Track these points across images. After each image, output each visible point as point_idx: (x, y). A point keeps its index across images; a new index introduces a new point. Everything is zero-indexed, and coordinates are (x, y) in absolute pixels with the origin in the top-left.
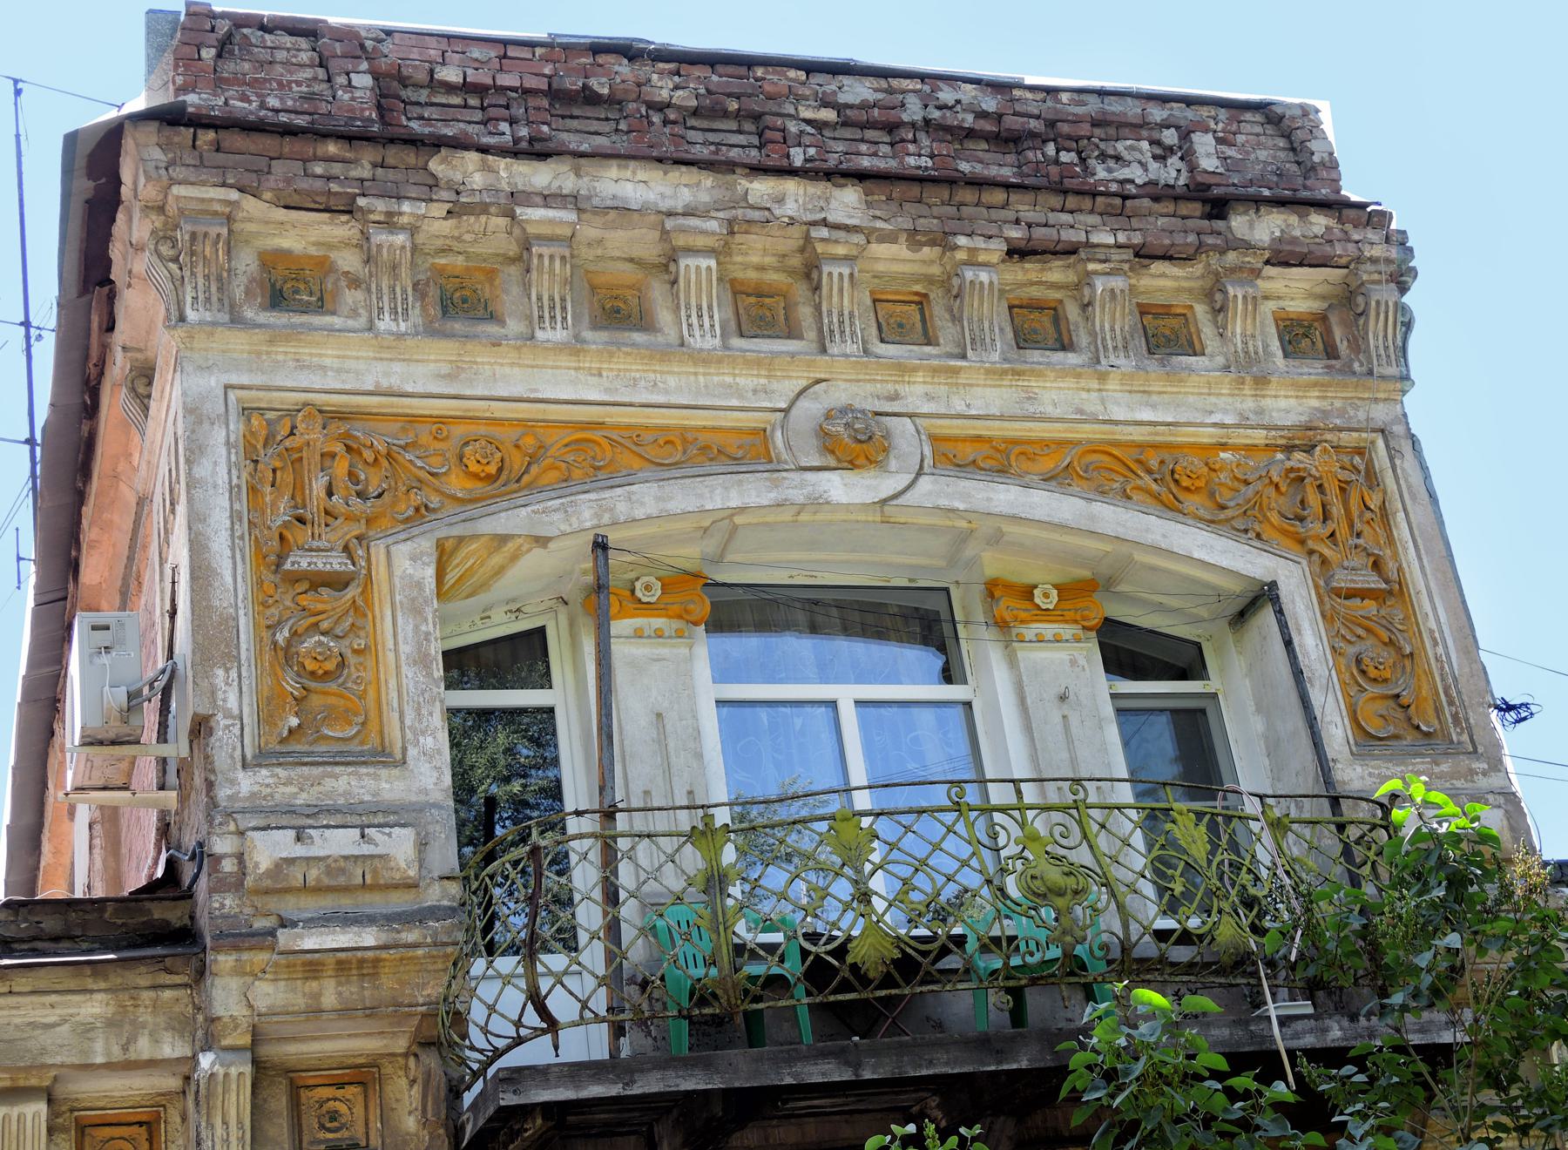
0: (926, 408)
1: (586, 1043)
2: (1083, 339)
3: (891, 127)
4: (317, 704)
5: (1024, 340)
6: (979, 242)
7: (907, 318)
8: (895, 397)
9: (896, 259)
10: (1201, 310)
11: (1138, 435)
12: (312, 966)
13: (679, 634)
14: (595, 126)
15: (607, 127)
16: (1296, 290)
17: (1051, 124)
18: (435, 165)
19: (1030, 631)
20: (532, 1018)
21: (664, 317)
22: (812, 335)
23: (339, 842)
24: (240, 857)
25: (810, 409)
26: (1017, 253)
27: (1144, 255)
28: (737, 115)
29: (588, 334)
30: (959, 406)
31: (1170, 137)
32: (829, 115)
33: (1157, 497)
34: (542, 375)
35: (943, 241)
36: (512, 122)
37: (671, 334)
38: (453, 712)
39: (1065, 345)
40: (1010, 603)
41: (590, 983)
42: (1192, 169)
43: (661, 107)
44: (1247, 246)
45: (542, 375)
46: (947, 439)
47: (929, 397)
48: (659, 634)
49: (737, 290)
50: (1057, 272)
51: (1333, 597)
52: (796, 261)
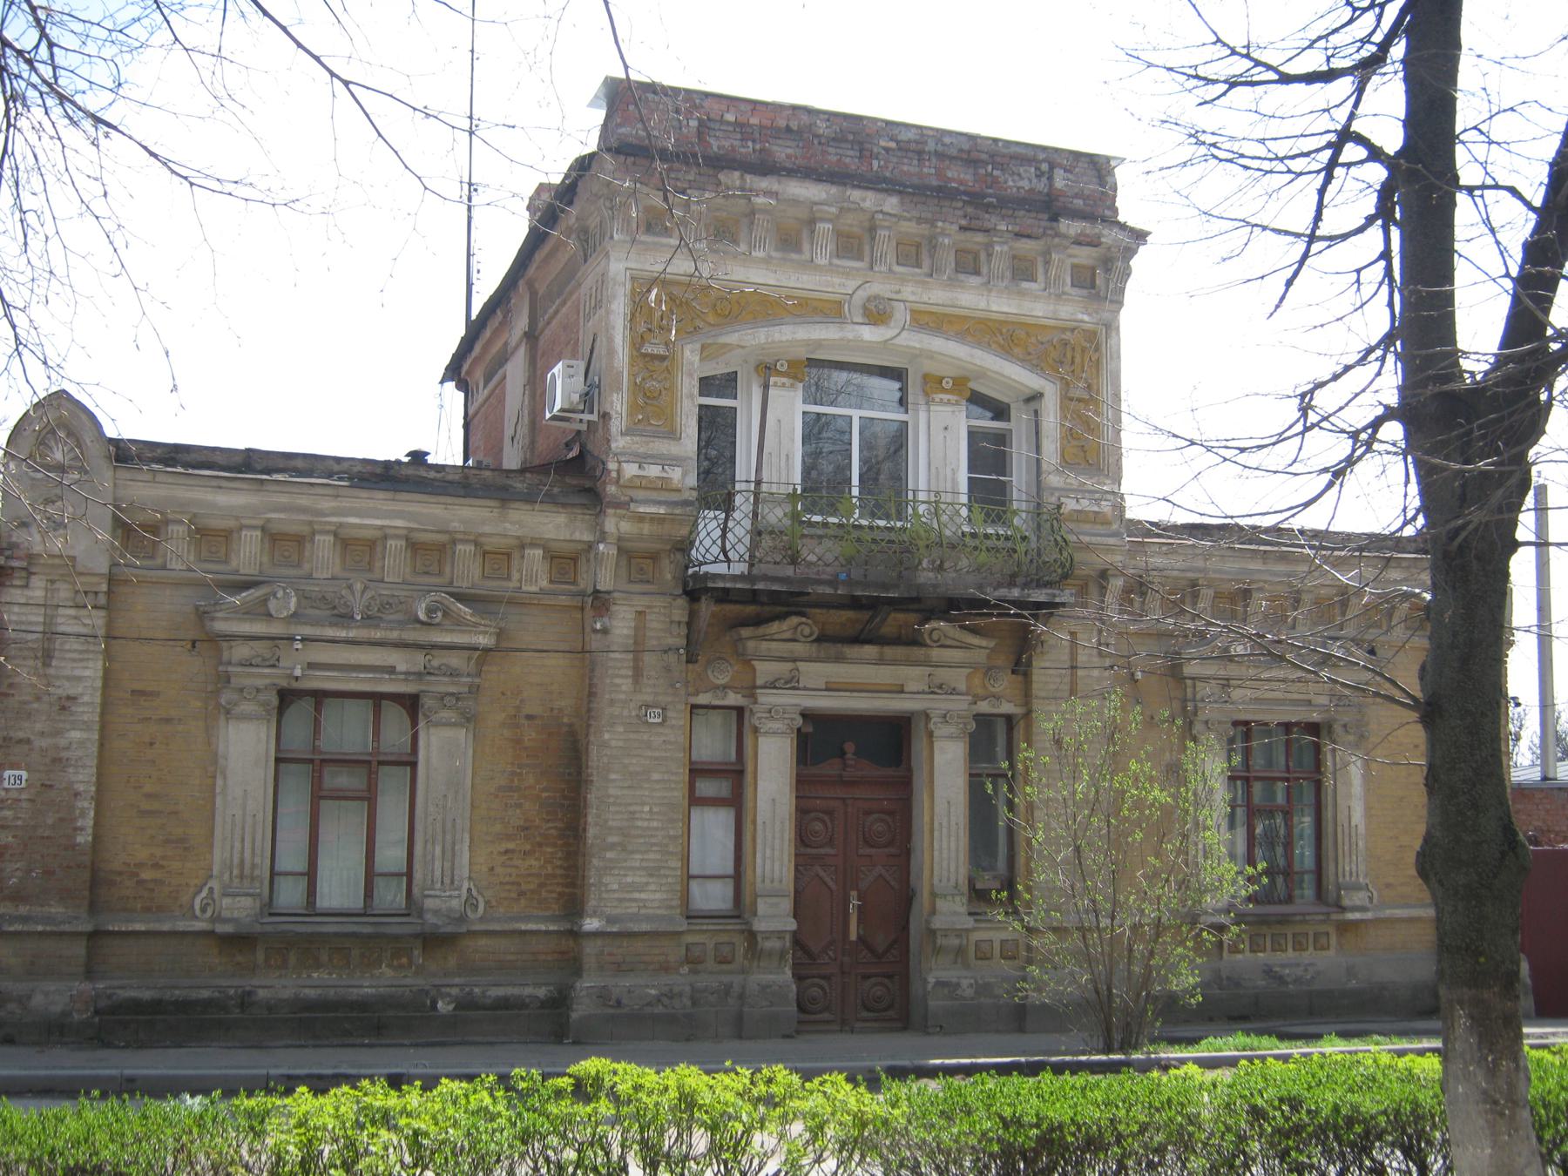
0: (912, 298)
1: (739, 568)
2: (984, 270)
3: (920, 153)
4: (652, 408)
5: (960, 268)
6: (947, 225)
7: (912, 254)
8: (899, 292)
9: (909, 227)
10: (1040, 259)
11: (1002, 317)
12: (641, 518)
13: (792, 386)
14: (789, 143)
15: (793, 144)
16: (1084, 255)
17: (992, 156)
18: (721, 177)
19: (938, 397)
20: (722, 557)
21: (806, 247)
22: (867, 259)
23: (653, 471)
24: (618, 472)
25: (861, 295)
26: (962, 229)
27: (1019, 235)
28: (852, 142)
29: (774, 254)
30: (925, 299)
31: (1044, 167)
32: (893, 145)
33: (1002, 347)
34: (753, 272)
35: (932, 223)
36: (754, 141)
37: (807, 256)
38: (701, 406)
39: (977, 272)
40: (932, 384)
41: (743, 532)
42: (1051, 185)
43: (818, 136)
44: (1065, 237)
45: (753, 272)
46: (920, 312)
47: (913, 293)
48: (784, 385)
49: (839, 234)
50: (980, 238)
51: (1066, 398)
52: (866, 224)
